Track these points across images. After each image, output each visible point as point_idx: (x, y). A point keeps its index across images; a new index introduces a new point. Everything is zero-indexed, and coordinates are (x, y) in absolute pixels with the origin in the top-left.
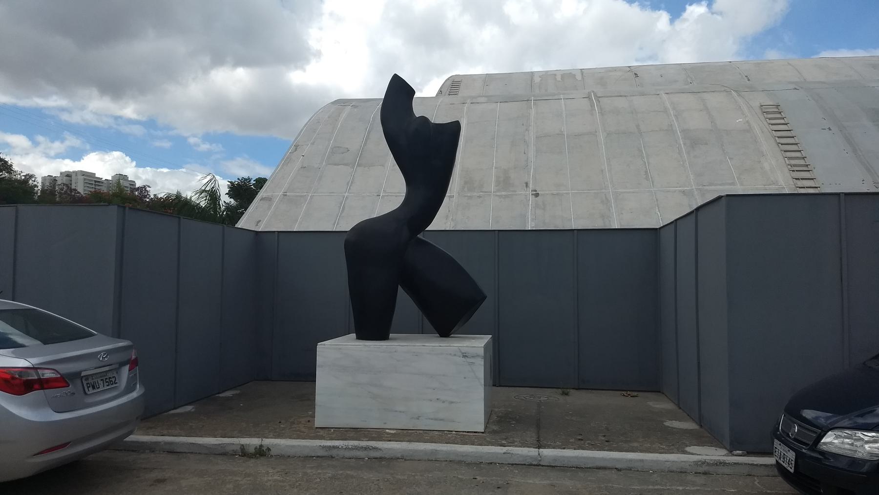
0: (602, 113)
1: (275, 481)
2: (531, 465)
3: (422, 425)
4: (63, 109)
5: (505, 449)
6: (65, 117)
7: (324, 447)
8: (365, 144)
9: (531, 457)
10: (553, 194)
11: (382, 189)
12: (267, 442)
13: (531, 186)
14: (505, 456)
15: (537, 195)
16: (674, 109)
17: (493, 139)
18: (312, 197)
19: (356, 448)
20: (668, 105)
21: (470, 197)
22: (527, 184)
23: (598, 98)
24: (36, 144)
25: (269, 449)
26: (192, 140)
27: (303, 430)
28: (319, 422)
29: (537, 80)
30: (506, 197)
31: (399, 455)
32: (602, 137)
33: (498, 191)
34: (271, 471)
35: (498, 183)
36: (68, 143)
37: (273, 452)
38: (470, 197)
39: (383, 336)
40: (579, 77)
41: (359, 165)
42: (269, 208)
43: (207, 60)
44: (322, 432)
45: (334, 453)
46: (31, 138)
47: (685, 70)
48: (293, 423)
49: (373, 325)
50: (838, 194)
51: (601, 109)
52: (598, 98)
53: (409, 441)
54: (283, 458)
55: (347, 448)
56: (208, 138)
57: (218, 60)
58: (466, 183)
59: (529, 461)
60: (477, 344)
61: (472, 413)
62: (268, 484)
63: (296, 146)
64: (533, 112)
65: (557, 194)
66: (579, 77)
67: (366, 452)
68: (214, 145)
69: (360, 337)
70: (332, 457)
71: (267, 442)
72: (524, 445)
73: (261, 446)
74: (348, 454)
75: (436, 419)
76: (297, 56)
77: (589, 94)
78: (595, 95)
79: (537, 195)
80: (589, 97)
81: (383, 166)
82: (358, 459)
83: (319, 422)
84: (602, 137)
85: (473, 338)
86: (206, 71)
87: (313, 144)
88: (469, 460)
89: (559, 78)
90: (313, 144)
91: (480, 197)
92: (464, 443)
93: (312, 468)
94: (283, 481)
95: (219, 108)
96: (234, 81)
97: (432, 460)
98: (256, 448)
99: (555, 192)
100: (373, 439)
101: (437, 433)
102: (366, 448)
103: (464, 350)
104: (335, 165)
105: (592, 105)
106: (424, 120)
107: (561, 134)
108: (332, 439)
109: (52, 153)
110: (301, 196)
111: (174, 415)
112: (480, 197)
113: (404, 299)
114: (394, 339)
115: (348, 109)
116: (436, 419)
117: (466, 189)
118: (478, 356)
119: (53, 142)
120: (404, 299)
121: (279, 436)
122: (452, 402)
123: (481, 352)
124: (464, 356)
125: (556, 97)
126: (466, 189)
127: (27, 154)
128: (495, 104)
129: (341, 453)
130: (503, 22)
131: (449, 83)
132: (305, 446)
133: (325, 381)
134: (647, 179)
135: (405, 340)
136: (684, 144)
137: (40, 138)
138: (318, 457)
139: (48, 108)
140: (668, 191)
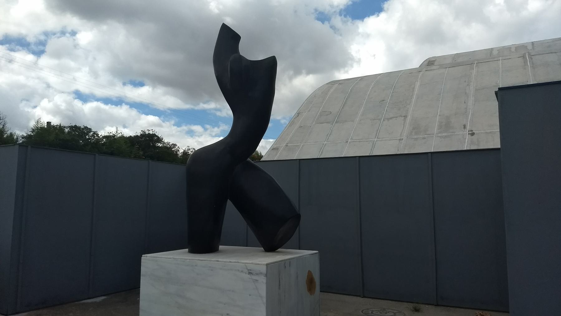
0: (534, 66)
4: (216, 109)
6: (218, 114)
10: (487, 133)
13: (468, 127)
15: (473, 134)
17: (440, 94)
22: (465, 127)
24: (206, 129)
29: (495, 53)
30: (446, 137)
33: (440, 133)
35: (440, 127)
36: (221, 128)
38: (416, 139)
41: (336, 122)
42: (276, 155)
46: (203, 127)
49: (204, 240)
52: (531, 56)
58: (414, 129)
64: (474, 72)
65: (490, 133)
69: (194, 251)
77: (525, 54)
79: (473, 134)
80: (524, 57)
86: (291, 79)
87: (309, 111)
90: (309, 111)
91: (424, 138)
99: (489, 131)
105: (525, 62)
109: (214, 134)
110: (296, 146)
111: (84, 303)
112: (424, 138)
114: (224, 252)
118: (261, 273)
119: (213, 128)
123: (264, 269)
124: (250, 273)
125: (496, 59)
127: (202, 135)
130: (485, 21)
131: (426, 63)
133: (147, 288)
137: (208, 126)
139: (210, 110)
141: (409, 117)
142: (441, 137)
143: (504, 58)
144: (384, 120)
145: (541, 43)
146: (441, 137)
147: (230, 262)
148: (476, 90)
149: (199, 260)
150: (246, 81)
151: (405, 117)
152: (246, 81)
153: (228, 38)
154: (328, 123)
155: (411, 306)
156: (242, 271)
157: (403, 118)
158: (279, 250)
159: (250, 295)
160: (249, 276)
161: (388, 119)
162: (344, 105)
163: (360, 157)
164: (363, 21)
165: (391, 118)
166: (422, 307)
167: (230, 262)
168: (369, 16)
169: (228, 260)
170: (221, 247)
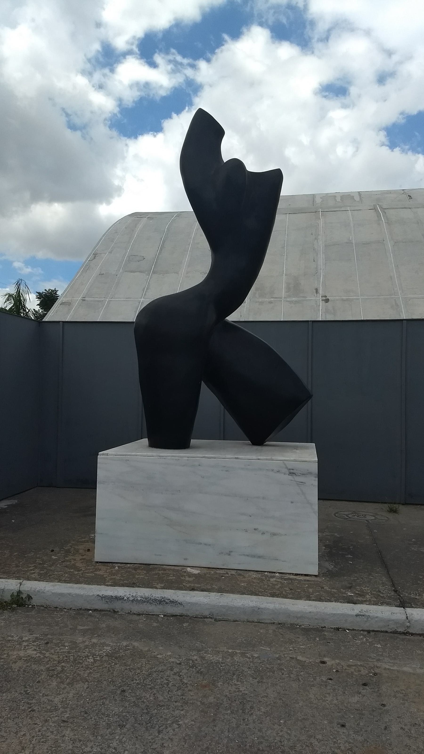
0: (389, 223)
1: (29, 659)
2: (395, 632)
3: (235, 563)
5: (358, 608)
7: (103, 598)
8: (160, 253)
9: (396, 622)
10: (343, 300)
12: (30, 586)
13: (321, 292)
14: (358, 619)
17: (283, 247)
18: (109, 302)
19: (147, 600)
21: (261, 303)
22: (317, 291)
25: (29, 597)
26: (16, 265)
27: (79, 565)
28: (100, 554)
29: (318, 200)
30: (296, 302)
31: (206, 613)
32: (389, 245)
33: (289, 296)
34: (27, 637)
35: (288, 289)
37: (35, 601)
38: (261, 303)
39: (180, 442)
40: (357, 198)
41: (154, 272)
43: (27, 195)
44: (102, 571)
45: (117, 606)
48: (68, 552)
49: (170, 430)
50: (308, 321)
53: (221, 591)
54: (49, 609)
55: (135, 601)
56: (31, 262)
57: (37, 196)
59: (392, 627)
60: (306, 456)
61: (300, 549)
62: (16, 667)
63: (95, 255)
64: (321, 222)
65: (347, 300)
66: (357, 198)
67: (161, 607)
68: (35, 269)
70: (115, 612)
71: (30, 586)
72: (379, 601)
73: (19, 592)
74: (136, 608)
75: (253, 556)
76: (105, 193)
78: (381, 207)
79: (327, 301)
80: (375, 209)
81: (177, 273)
82: (149, 615)
83: (100, 554)
84: (389, 245)
85: (296, 448)
86: (26, 206)
87: (111, 252)
88: (306, 623)
89: (338, 199)
90: (111, 252)
91: (271, 302)
92: (297, 596)
93: (84, 633)
94: (38, 661)
95: (37, 238)
96: (51, 215)
97: (254, 620)
98: (12, 595)
99: (344, 298)
100: (169, 586)
101: (254, 575)
102: (161, 602)
104: (132, 272)
105: (379, 216)
106: (237, 164)
107: (349, 243)
108: (115, 584)
112: (271, 302)
114: (197, 447)
115: (144, 220)
116: (253, 556)
117: (257, 295)
118: (310, 473)
121: (44, 577)
122: (274, 534)
124: (291, 474)
125: (343, 209)
126: (257, 295)
128: (284, 216)
129: (127, 607)
132: (78, 595)
135: (211, 448)
138: (95, 610)
142: (287, 301)
143: (353, 209)
145: (333, 196)
146: (291, 302)
147: (259, 459)
148: (326, 246)
149: (204, 457)
154: (141, 272)
155: (386, 506)
156: (278, 472)
158: (267, 443)
159: (292, 502)
160: (290, 477)
162: (161, 249)
166: (402, 509)
167: (259, 459)
169: (254, 457)
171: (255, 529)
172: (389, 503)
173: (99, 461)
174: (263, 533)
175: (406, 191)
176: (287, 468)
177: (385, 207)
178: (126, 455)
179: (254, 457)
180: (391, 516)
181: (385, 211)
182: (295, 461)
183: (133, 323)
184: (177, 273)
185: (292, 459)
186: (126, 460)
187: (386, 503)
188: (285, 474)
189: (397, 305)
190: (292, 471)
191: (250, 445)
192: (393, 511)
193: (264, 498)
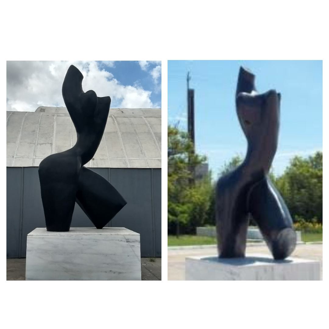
0: (119, 124)
10: (101, 159)
11: (64, 138)
16: (149, 123)
17: (70, 132)
20: (147, 122)
23: (115, 117)
32: (120, 134)
39: (66, 229)
47: (143, 111)
50: (108, 168)
51: (117, 122)
81: (15, 143)
84: (120, 134)
85: (120, 229)
103: (127, 237)
105: (114, 120)
106: (92, 93)
113: (78, 210)
114: (71, 231)
118: (137, 241)
120: (78, 210)
122: (120, 273)
124: (127, 242)
134: (142, 154)
136: (156, 139)
140: (152, 159)
141: (54, 145)
144: (37, 145)
147: (111, 235)
150: (259, 113)
151: (51, 144)
152: (259, 113)
153: (74, 76)
157: (50, 145)
158: (104, 228)
160: (127, 243)
161: (41, 144)
163: (24, 167)
164: (279, 95)
165: (42, 144)
168: (128, 86)
169: (109, 234)
170: (71, 228)
171: (110, 271)
172: (150, 257)
173: (28, 239)
174: (114, 273)
175: (120, 109)
176: (125, 239)
177: (115, 116)
178: (41, 235)
179: (109, 234)
180: (152, 263)
181: (116, 118)
182: (129, 235)
183: (37, 167)
184: (15, 143)
185: (128, 234)
186: (43, 238)
187: (148, 257)
188: (124, 242)
189: (125, 162)
190: (128, 240)
191: (96, 229)
192: (152, 261)
193: (114, 255)
